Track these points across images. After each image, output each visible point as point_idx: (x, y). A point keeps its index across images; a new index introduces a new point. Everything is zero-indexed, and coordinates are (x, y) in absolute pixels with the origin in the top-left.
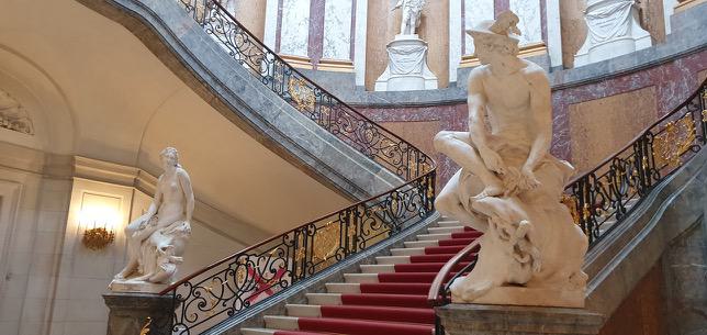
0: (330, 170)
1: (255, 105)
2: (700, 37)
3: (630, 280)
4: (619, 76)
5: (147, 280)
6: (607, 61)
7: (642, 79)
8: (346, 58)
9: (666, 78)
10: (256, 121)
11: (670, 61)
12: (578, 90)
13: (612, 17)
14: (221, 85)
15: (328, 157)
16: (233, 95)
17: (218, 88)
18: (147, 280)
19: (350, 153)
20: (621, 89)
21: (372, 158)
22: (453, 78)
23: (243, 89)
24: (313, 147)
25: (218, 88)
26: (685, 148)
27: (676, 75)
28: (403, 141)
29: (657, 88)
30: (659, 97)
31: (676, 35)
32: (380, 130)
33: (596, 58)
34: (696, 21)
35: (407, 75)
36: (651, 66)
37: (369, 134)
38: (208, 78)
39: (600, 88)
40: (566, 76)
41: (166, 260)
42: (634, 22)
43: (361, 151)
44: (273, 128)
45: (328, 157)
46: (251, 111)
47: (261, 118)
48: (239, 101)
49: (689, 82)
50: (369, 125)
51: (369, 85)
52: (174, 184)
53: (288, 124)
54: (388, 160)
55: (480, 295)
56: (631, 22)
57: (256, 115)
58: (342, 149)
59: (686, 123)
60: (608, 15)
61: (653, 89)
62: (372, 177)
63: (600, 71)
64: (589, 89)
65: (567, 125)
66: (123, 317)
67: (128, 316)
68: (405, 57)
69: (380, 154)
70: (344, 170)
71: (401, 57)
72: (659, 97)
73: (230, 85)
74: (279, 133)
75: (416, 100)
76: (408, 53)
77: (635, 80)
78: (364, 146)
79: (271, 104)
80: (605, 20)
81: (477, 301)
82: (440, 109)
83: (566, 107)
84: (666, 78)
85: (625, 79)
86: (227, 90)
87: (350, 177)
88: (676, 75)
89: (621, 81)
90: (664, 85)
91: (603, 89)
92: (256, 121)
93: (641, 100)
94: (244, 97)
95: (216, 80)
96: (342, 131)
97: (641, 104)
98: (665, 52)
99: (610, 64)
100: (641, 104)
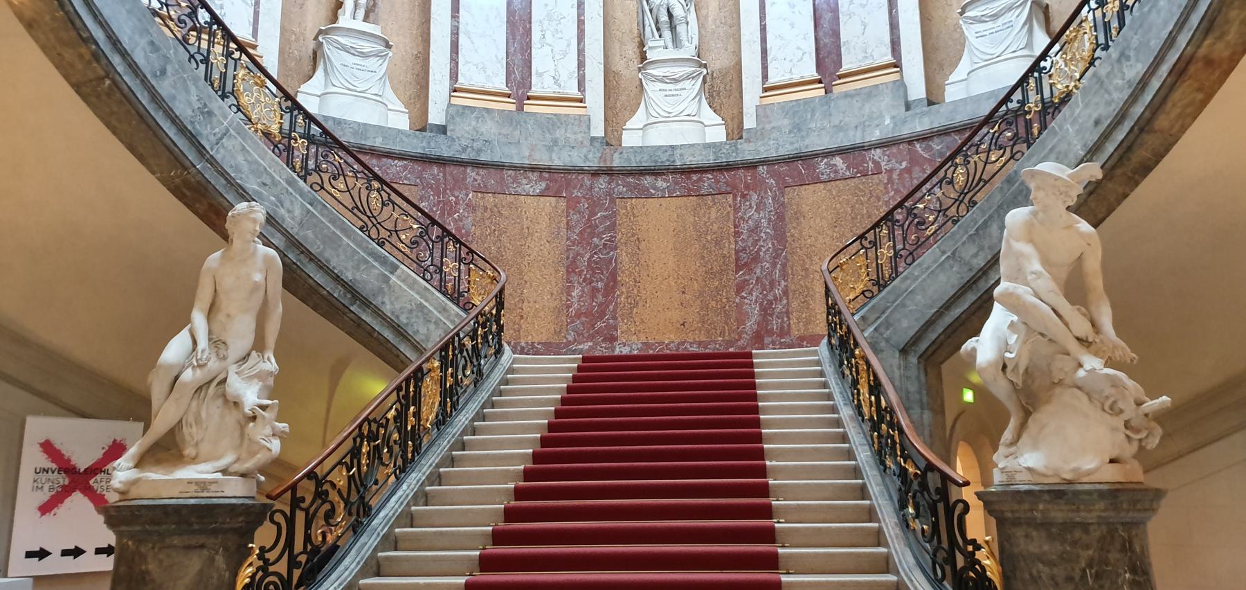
0: (312, 258)
1: (183, 110)
2: (792, 143)
3: (154, 469)
4: (687, 171)
5: (224, 472)
6: (673, 147)
7: (717, 182)
8: (573, 91)
9: (747, 187)
10: (182, 143)
11: (752, 165)
12: (630, 179)
13: (680, 86)
14: (124, 54)
15: (310, 233)
16: (144, 81)
17: (116, 60)
18: (224, 472)
19: (345, 230)
20: (689, 190)
21: (381, 245)
22: (436, 116)
23: (163, 72)
24: (282, 211)
25: (116, 60)
26: (858, 291)
27: (758, 185)
28: (434, 222)
29: (735, 199)
30: (736, 210)
31: (759, 133)
32: (394, 197)
33: (659, 137)
34: (786, 122)
35: (360, 95)
36: (730, 167)
37: (375, 203)
38: (98, 34)
39: (661, 183)
40: (616, 155)
41: (268, 431)
42: (704, 101)
43: (361, 229)
44: (212, 161)
45: (310, 233)
46: (174, 120)
47: (193, 139)
48: (155, 96)
49: (773, 199)
50: (376, 184)
51: (611, 141)
52: (258, 277)
53: (240, 159)
54: (407, 250)
55: (1089, 473)
56: (700, 101)
57: (182, 130)
58: (333, 221)
59: (861, 261)
60: (676, 81)
61: (730, 198)
62: (386, 280)
63: (663, 159)
64: (648, 181)
65: (612, 228)
66: (189, 548)
67: (202, 546)
68: (357, 60)
69: (394, 239)
70: (337, 262)
71: (351, 60)
72: (736, 210)
73: (139, 58)
74: (223, 174)
75: (378, 142)
76: (364, 55)
77: (708, 180)
78: (369, 222)
79: (210, 113)
80: (671, 86)
81: (1085, 480)
82: (418, 167)
83: (613, 201)
84: (747, 187)
85: (695, 177)
86: (133, 67)
87: (348, 276)
88: (758, 185)
89: (689, 178)
90: (744, 196)
91: (665, 185)
92: (182, 143)
93: (714, 210)
94: (164, 88)
95: (115, 42)
96: (327, 186)
97: (713, 215)
98: (748, 151)
99: (678, 152)
100: (713, 215)
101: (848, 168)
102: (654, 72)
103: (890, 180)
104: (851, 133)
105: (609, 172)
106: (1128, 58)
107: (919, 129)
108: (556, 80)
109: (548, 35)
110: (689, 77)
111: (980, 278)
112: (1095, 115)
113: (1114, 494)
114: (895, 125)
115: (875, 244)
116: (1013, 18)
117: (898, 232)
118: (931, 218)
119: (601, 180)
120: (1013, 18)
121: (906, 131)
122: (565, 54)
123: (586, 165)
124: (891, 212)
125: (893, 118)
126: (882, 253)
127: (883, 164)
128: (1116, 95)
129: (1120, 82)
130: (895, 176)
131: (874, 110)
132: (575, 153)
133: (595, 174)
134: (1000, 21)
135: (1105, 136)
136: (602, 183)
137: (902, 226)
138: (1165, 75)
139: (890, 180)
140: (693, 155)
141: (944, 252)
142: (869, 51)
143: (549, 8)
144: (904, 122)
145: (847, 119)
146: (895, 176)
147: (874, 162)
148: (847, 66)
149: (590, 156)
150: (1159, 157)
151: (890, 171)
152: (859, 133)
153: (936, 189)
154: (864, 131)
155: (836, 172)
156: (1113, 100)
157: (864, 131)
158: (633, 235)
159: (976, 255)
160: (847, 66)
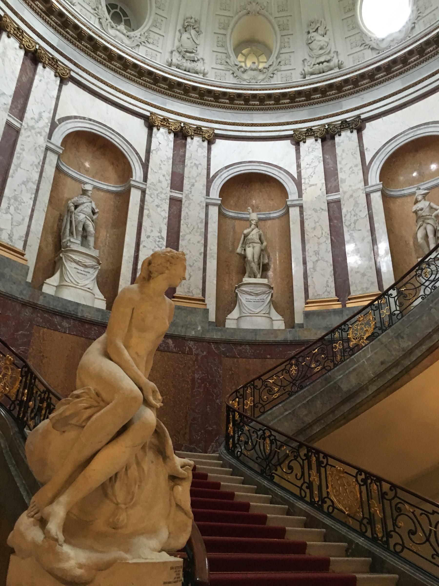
13: (87, 270)
64: (57, 319)
91: (67, 325)
101: (175, 347)
102: (73, 257)
103: (196, 360)
104: (180, 328)
105: (34, 307)
106: (402, 338)
107: (215, 337)
108: (10, 238)
109: (12, 208)
110: (92, 267)
111: (308, 428)
112: (382, 359)
113: (45, 527)
114: (203, 331)
115: (243, 397)
116: (265, 298)
117: (257, 392)
118: (276, 389)
119: (27, 310)
120: (265, 298)
121: (208, 336)
122: (19, 224)
123: (20, 297)
124: (253, 380)
125: (202, 327)
126: (247, 404)
127: (194, 350)
128: (394, 353)
129: (397, 347)
130: (199, 358)
131: (193, 320)
132: (14, 287)
133: (25, 304)
134: (259, 298)
135: (387, 370)
136: (27, 313)
137: (259, 389)
138: (424, 350)
139: (196, 360)
140: (89, 313)
141: (286, 410)
142: (191, 289)
143: (16, 193)
144: (208, 331)
145: (178, 320)
146: (199, 358)
147: (189, 347)
148: (353, 295)
149: (25, 292)
150: (402, 386)
151: (197, 355)
152: (184, 330)
153: (280, 374)
154: (186, 329)
155: (168, 347)
156: (392, 355)
157: (186, 329)
158: (40, 352)
159: (306, 415)
160: (353, 295)
